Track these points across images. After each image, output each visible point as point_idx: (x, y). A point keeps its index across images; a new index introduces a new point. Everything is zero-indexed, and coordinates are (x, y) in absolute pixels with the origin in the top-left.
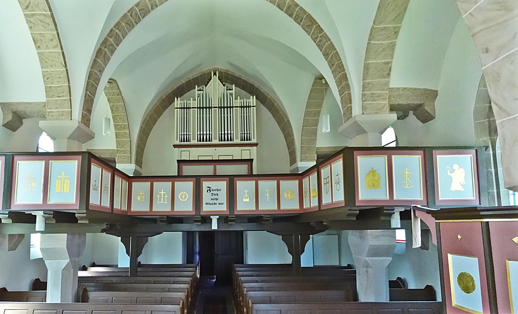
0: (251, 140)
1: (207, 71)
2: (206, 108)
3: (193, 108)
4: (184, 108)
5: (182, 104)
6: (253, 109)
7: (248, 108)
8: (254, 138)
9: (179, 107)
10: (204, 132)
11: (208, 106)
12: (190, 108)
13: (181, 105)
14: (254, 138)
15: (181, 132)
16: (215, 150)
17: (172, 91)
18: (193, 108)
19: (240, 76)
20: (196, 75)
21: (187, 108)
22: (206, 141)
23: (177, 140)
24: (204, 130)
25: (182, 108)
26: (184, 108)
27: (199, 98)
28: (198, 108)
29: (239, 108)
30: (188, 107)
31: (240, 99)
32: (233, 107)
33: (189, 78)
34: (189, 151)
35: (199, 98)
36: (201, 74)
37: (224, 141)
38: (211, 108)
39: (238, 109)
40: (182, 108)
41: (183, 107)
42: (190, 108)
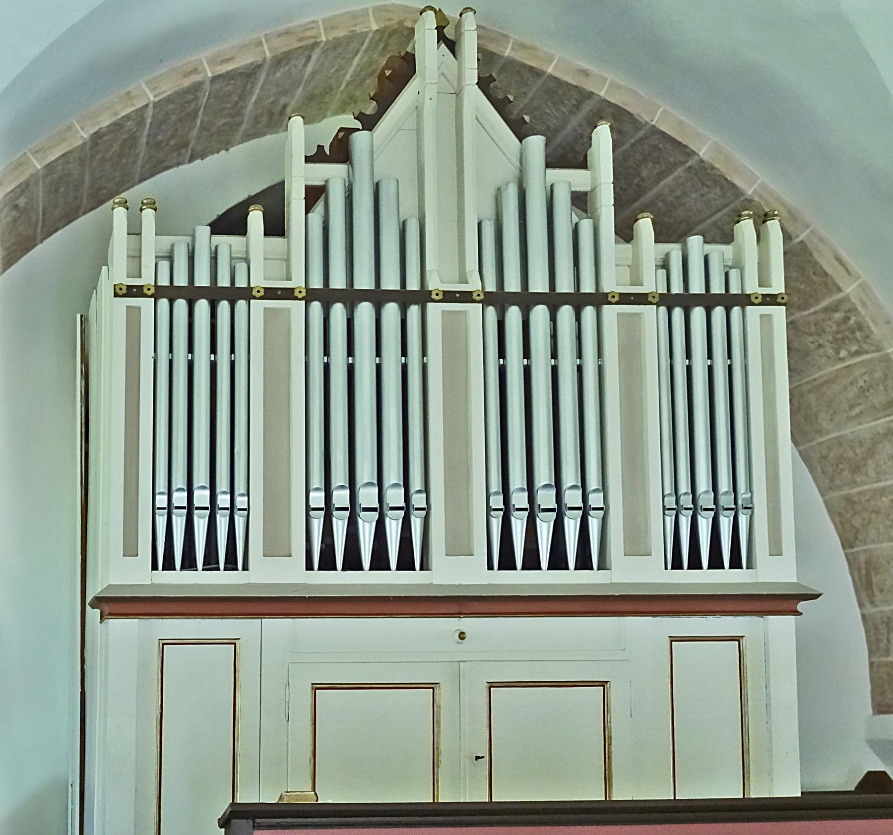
0: (245, 568)
1: (331, 24)
2: (378, 298)
3: (271, 294)
4: (687, 301)
5: (170, 258)
6: (766, 320)
7: (224, 307)
8: (776, 550)
9: (147, 279)
10: (197, 493)
11: (565, 286)
12: (247, 294)
13: (164, 265)
14: (776, 550)
15: (162, 486)
16: (462, 636)
17: (52, 158)
18: (271, 294)
19: (585, 73)
20: (244, 48)
21: (708, 301)
22: (380, 562)
23: (130, 550)
24: (196, 484)
25: (170, 293)
26: (191, 294)
27: (316, 216)
28: (311, 296)
29: (474, 310)
30: (224, 282)
31: (659, 238)
32: (423, 297)
33: (195, 71)
34: (233, 642)
35: (316, 216)
36: (283, 45)
37: (183, 568)
38: (423, 297)
39: (464, 313)
40: (170, 293)
41: (181, 280)
42: (247, 294)
